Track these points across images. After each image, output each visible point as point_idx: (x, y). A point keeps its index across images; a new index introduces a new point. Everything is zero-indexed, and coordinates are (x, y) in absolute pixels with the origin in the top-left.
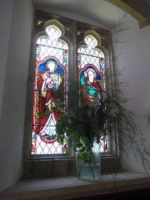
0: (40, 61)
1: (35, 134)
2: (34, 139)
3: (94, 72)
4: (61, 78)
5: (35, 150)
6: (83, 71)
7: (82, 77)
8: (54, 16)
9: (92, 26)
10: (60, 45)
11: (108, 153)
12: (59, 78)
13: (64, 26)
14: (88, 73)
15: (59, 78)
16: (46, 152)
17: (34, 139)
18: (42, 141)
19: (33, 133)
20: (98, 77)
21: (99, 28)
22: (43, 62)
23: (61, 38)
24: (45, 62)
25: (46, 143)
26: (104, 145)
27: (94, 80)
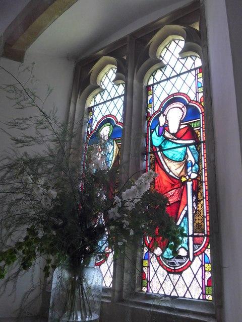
0: (154, 113)
1: (148, 252)
2: (147, 262)
3: (181, 107)
4: (118, 145)
5: (148, 287)
6: (159, 115)
7: (155, 129)
8: (98, 53)
9: (159, 19)
10: (189, 63)
11: (205, 304)
12: (113, 148)
13: (184, 27)
14: (166, 116)
15: (113, 148)
16: (168, 289)
17: (147, 262)
18: (160, 267)
19: (146, 250)
20: (192, 113)
21: (173, 13)
22: (188, 103)
23: (117, 79)
24: (190, 104)
25: (169, 272)
26: (203, 279)
27: (180, 125)
